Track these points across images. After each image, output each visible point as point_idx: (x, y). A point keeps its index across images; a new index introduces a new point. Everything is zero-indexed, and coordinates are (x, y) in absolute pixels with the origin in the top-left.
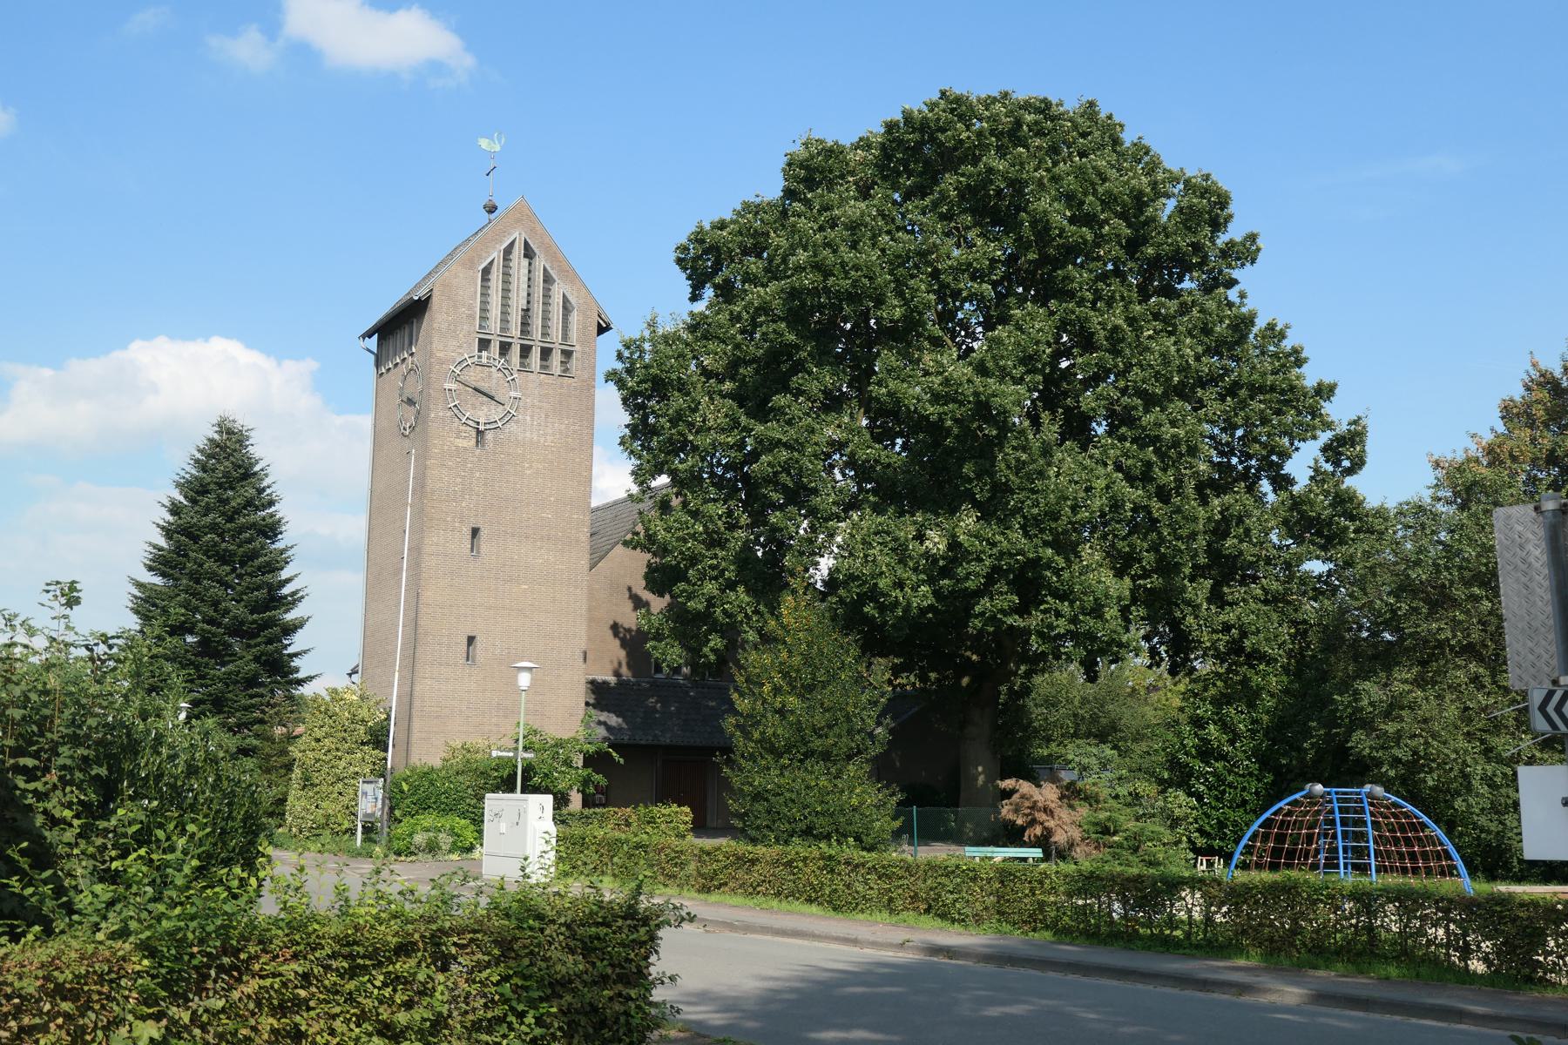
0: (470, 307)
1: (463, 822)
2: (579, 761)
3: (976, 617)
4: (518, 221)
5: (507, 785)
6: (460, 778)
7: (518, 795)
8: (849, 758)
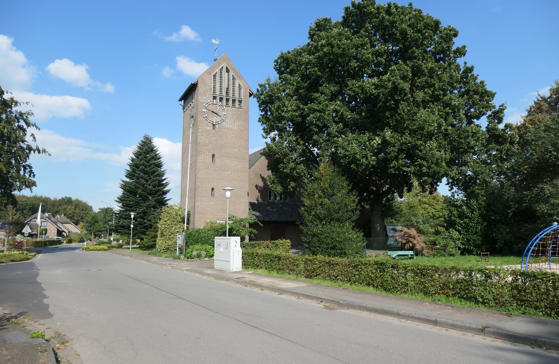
0: (210, 86)
1: (210, 247)
2: (247, 225)
3: (391, 168)
4: (224, 60)
5: (224, 234)
6: (209, 232)
7: (227, 237)
8: (347, 220)
